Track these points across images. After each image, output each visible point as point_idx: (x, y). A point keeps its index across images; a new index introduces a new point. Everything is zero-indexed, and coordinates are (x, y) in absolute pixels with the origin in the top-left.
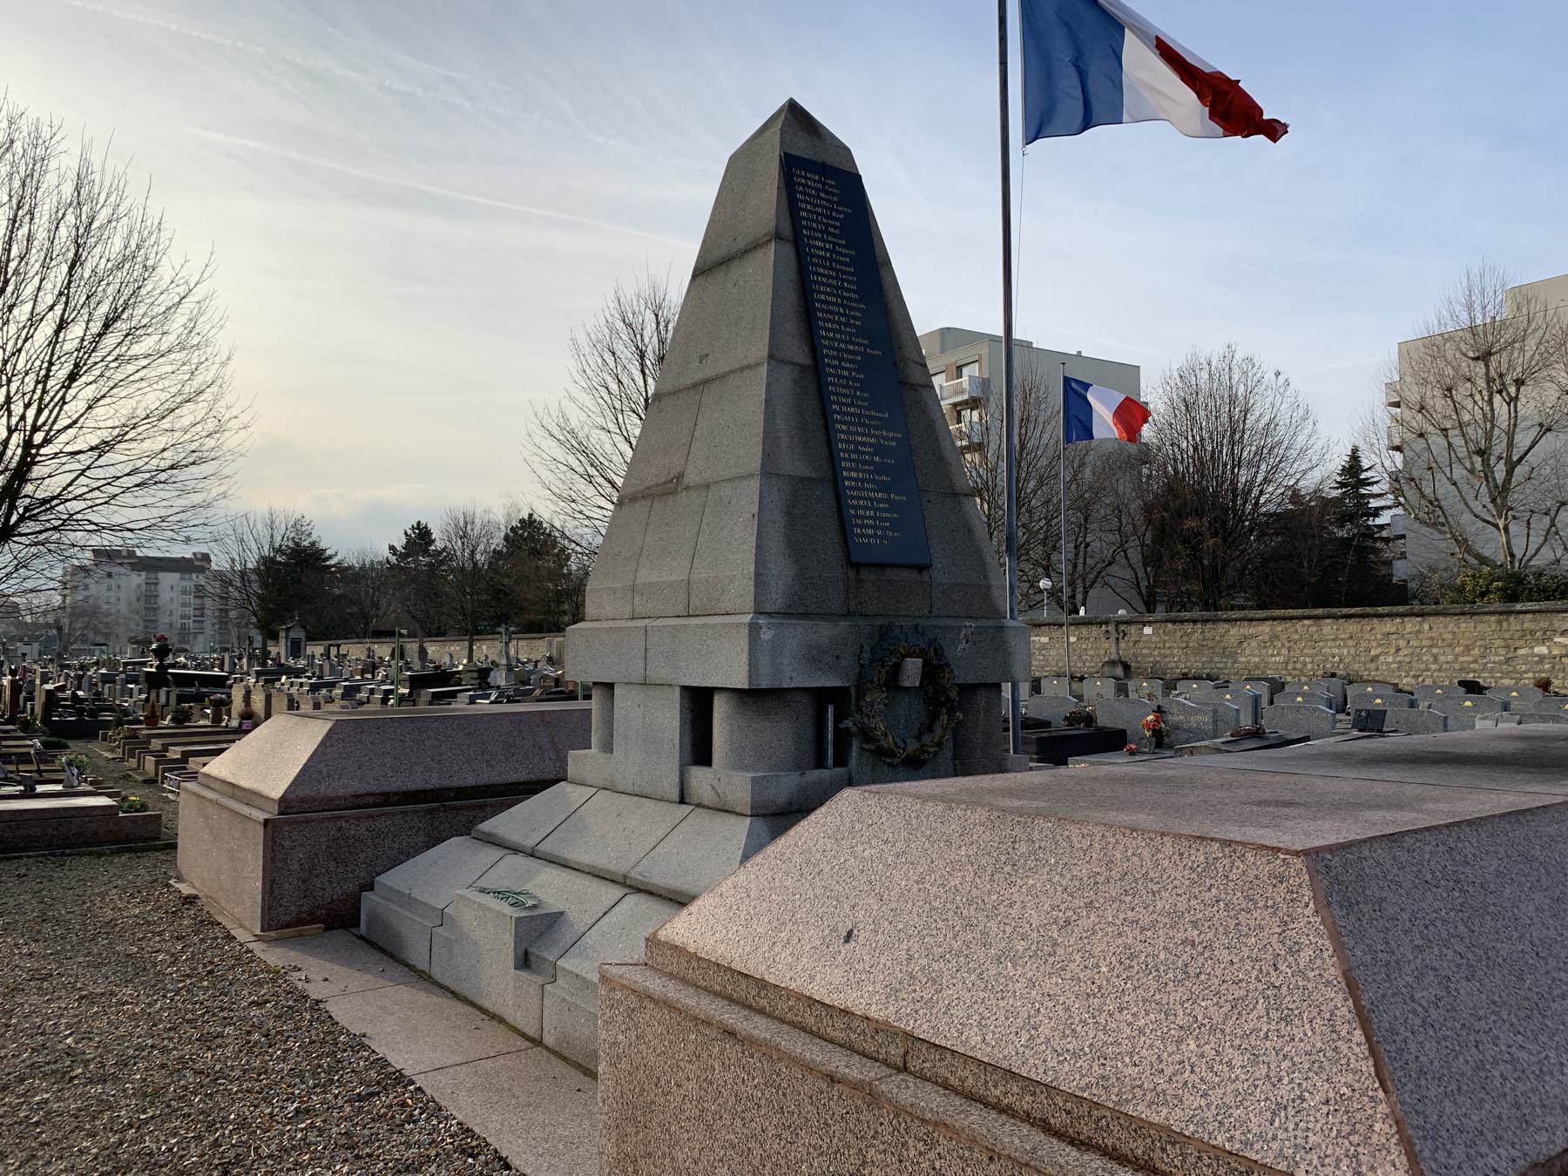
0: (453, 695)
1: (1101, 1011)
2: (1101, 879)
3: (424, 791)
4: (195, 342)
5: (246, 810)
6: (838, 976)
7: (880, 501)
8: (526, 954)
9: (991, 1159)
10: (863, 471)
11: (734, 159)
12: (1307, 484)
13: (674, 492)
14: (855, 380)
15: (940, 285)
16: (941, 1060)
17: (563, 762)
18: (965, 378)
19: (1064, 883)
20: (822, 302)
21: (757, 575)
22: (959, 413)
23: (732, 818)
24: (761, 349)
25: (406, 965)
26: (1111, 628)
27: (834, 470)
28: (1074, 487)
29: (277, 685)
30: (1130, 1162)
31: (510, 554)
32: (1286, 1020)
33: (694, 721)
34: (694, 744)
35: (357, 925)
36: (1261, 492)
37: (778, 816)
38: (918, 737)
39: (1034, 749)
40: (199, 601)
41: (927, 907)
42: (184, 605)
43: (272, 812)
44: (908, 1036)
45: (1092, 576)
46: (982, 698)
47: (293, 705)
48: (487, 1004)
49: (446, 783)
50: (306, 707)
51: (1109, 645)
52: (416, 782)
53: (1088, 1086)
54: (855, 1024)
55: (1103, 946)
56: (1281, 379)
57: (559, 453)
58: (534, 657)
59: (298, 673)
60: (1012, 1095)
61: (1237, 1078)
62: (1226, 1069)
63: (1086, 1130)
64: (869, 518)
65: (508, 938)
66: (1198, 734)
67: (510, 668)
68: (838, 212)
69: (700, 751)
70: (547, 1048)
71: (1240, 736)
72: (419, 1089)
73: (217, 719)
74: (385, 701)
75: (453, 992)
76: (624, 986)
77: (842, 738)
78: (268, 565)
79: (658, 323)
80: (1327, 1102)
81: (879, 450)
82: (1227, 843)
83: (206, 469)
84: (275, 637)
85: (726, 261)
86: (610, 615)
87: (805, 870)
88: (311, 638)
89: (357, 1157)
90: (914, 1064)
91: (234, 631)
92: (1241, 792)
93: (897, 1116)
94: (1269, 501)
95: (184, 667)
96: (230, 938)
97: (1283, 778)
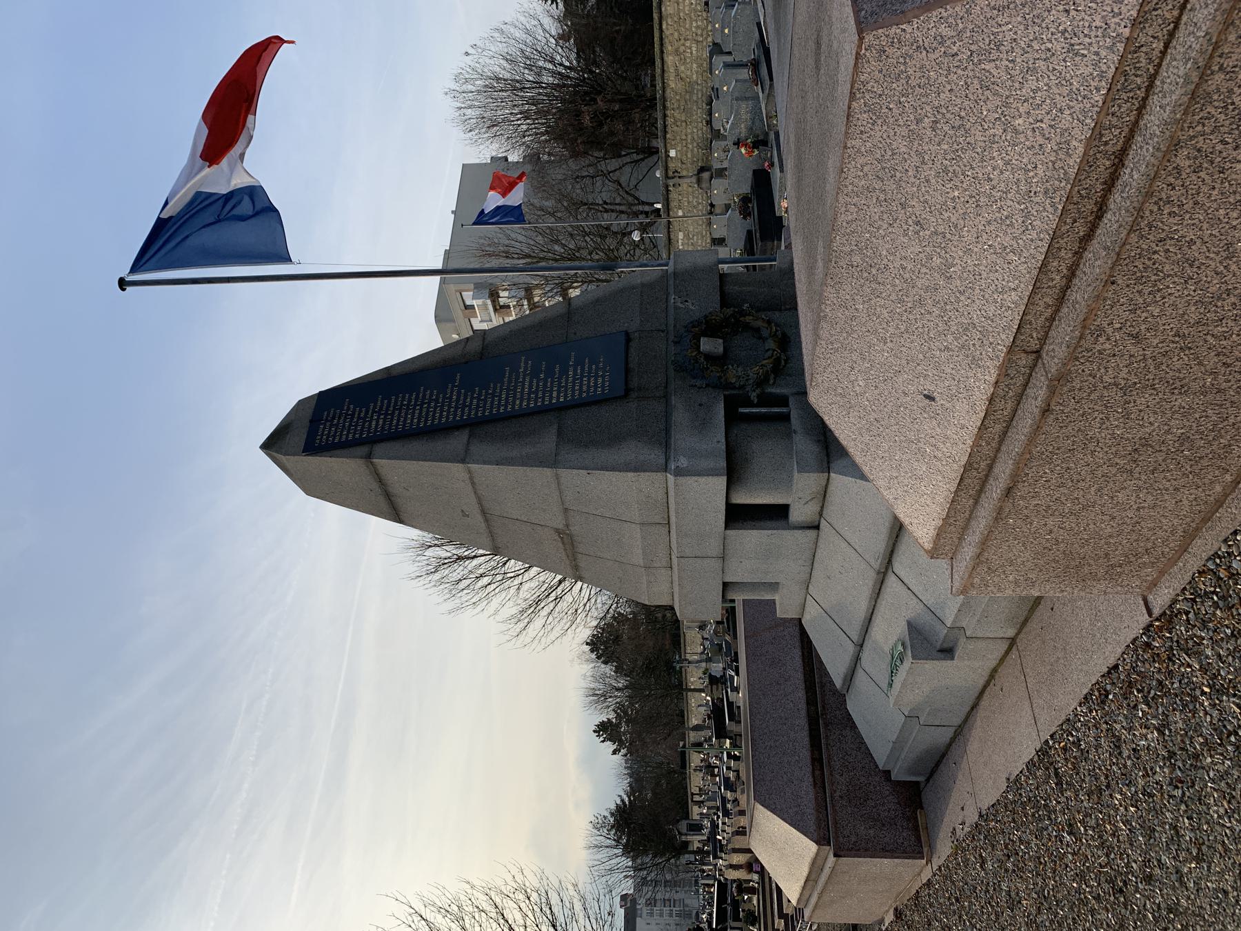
0: (730, 704)
1: (990, 196)
2: (882, 197)
3: (811, 730)
4: (456, 909)
5: (827, 871)
6: (961, 406)
7: (575, 374)
8: (941, 651)
9: (1113, 283)
10: (552, 387)
12: (554, 28)
13: (571, 536)
14: (480, 395)
15: (404, 328)
16: (1030, 323)
17: (785, 621)
18: (475, 303)
19: (885, 226)
20: (419, 422)
21: (636, 470)
22: (502, 307)
23: (831, 488)
24: (457, 469)
25: (950, 745)
26: (671, 182)
28: (559, 215)
29: (724, 842)
30: (1116, 171)
31: (618, 660)
32: (998, 46)
33: (753, 519)
34: (771, 518)
35: (917, 783)
36: (561, 64)
37: (829, 451)
38: (764, 340)
39: (769, 244)
40: (658, 903)
41: (906, 336)
42: (661, 915)
43: (829, 851)
44: (1010, 350)
45: (630, 199)
46: (732, 289)
47: (742, 832)
48: (981, 682)
49: (803, 712)
50: (743, 821)
51: (685, 183)
52: (803, 737)
53: (1053, 205)
54: (1001, 393)
55: (937, 194)
56: (471, 51)
57: (538, 622)
58: (699, 640)
59: (714, 826)
60: (1060, 266)
61: (1047, 85)
62: (1039, 94)
63: (1089, 206)
64: (589, 381)
65: (929, 665)
66: (756, 111)
67: (709, 660)
68: (348, 409)
69: (777, 514)
70: (1017, 634)
71: (757, 79)
72: (1052, 736)
73: (752, 891)
74: (736, 758)
75: (972, 709)
76: (970, 576)
77: (766, 400)
78: (630, 850)
79: (436, 545)
80: (1067, 11)
81: (535, 374)
82: (852, 96)
83: (554, 900)
84: (686, 844)
85: (388, 496)
87: (875, 433)
88: (687, 815)
89: (1108, 786)
90: (1034, 344)
91: (682, 876)
92: (808, 82)
93: (1077, 359)
94: (568, 59)
95: (710, 914)
96: (929, 884)
97: (795, 49)
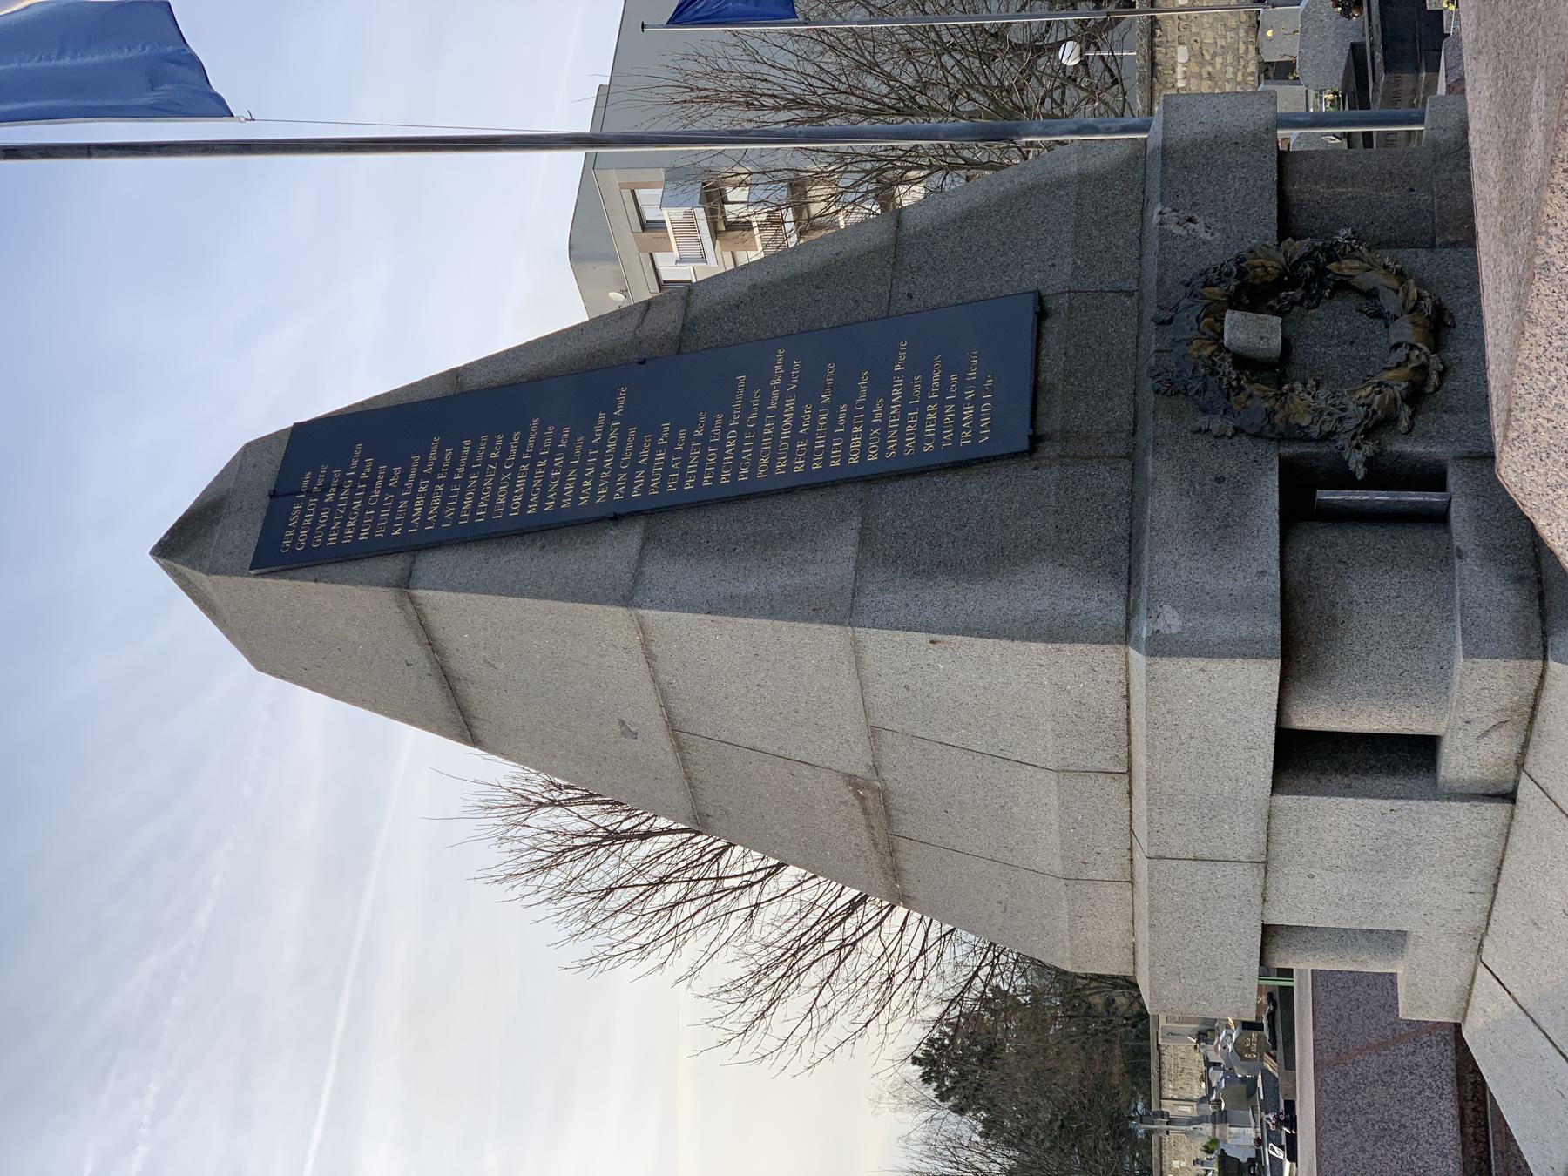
7: (907, 392)
10: (849, 425)
11: (262, 662)
13: (884, 795)
14: (673, 439)
17: (1419, 1029)
18: (666, 215)
21: (1051, 636)
22: (731, 227)
24: (612, 621)
27: (846, 482)
39: (1406, 77)
57: (797, 1002)
58: (1198, 1068)
64: (941, 415)
67: (1220, 1118)
69: (1412, 756)
77: (1381, 474)
79: (553, 803)
81: (807, 393)
85: (447, 679)
86: (1124, 926)
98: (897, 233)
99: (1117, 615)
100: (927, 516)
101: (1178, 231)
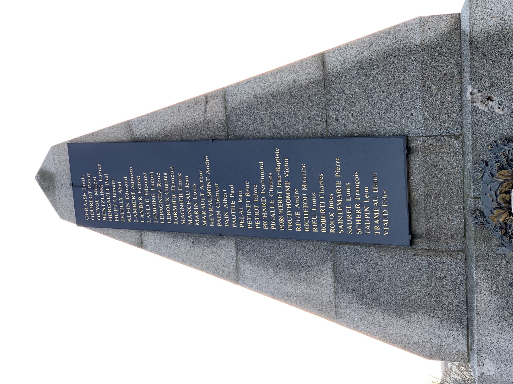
98: (323, 71)
99: (463, 348)
100: (364, 270)
101: (482, 107)
